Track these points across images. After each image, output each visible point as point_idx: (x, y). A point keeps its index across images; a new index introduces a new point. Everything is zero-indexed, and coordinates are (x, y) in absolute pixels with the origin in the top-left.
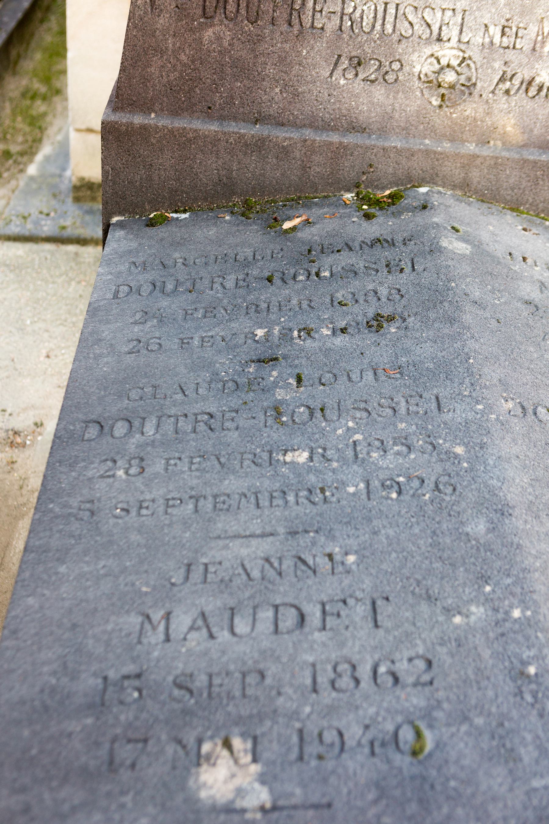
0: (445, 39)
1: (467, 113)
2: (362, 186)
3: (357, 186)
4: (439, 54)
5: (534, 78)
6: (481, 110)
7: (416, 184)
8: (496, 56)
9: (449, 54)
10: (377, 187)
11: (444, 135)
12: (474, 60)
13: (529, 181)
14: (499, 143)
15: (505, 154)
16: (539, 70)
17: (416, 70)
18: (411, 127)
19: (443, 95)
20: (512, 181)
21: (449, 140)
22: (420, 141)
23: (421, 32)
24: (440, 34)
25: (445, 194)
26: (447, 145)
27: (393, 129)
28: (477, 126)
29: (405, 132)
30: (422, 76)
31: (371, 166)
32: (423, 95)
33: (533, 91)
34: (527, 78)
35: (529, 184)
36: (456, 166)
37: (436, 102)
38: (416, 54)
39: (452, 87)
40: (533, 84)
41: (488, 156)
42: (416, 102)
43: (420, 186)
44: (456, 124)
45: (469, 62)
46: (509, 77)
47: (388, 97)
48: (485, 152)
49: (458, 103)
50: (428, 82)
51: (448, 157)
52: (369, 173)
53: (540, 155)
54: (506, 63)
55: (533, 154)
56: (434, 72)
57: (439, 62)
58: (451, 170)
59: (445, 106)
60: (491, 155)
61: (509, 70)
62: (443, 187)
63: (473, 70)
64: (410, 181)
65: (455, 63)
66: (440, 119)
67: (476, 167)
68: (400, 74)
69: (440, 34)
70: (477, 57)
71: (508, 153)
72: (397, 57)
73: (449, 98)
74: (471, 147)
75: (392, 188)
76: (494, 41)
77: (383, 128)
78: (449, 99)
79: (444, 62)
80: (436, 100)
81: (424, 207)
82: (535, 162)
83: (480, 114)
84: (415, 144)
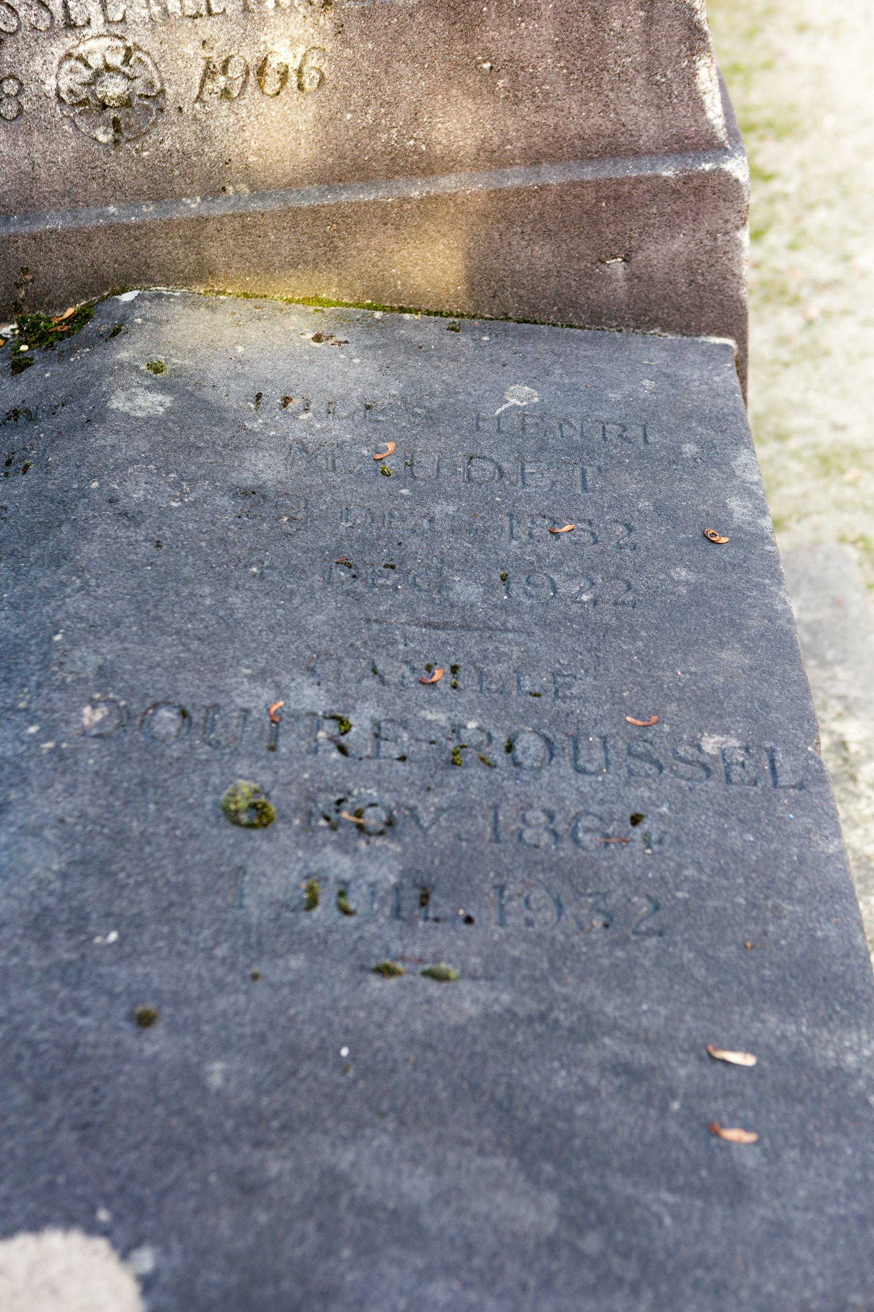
0: (80, 23)
1: (167, 145)
2: (25, 308)
3: (17, 308)
4: (82, 49)
5: (266, 59)
6: (188, 135)
7: (118, 288)
8: (182, 34)
9: (99, 49)
10: (50, 305)
11: (140, 192)
12: (145, 49)
13: (317, 246)
14: (244, 188)
15: (257, 206)
16: (269, 45)
17: (50, 84)
18: (75, 190)
19: (116, 122)
20: (285, 251)
21: (150, 199)
22: (99, 210)
23: (33, 19)
24: (67, 15)
25: (169, 297)
26: (148, 209)
27: (45, 198)
28: (192, 165)
29: (70, 197)
30: (64, 96)
31: (25, 271)
32: (77, 128)
33: (272, 83)
34: (253, 62)
35: (321, 251)
36: (174, 244)
37: (104, 136)
38: (39, 60)
39: (126, 103)
40: (268, 70)
41: (225, 216)
42: (68, 144)
43: (124, 291)
44: (153, 168)
45: (138, 54)
46: (219, 67)
47: (15, 144)
48: (220, 209)
49: (143, 130)
50: (80, 103)
51: (153, 231)
52: (27, 283)
53: (323, 195)
54: (204, 42)
55: (307, 196)
56: (83, 84)
57: (87, 65)
58: (169, 253)
59: (123, 140)
60: (230, 212)
61: (214, 54)
62: (168, 285)
63: (151, 67)
64: (105, 285)
65: (116, 60)
66: (118, 167)
67: (211, 238)
68: (23, 100)
69: (67, 15)
70: (148, 43)
71: (260, 204)
72: (7, 72)
73: (127, 124)
74: (194, 204)
75: (75, 303)
76: (170, 8)
77: (27, 199)
78: (128, 127)
79: (96, 62)
80: (105, 132)
81: (115, 333)
82: (315, 210)
83: (191, 143)
84: (89, 219)
